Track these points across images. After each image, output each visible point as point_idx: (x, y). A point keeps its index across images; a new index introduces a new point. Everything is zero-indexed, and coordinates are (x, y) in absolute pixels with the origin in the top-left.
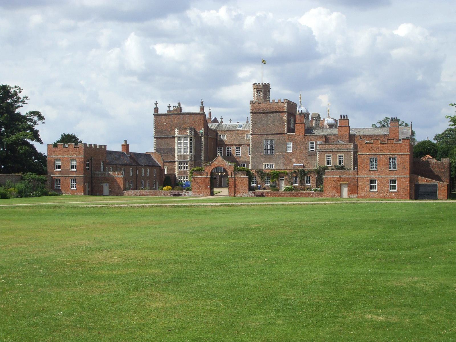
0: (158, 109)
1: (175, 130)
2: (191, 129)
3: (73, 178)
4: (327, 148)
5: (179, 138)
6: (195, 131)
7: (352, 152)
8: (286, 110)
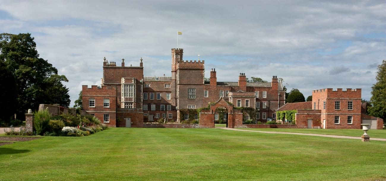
1: (122, 80)
2: (135, 79)
3: (106, 114)
4: (238, 95)
6: (137, 80)
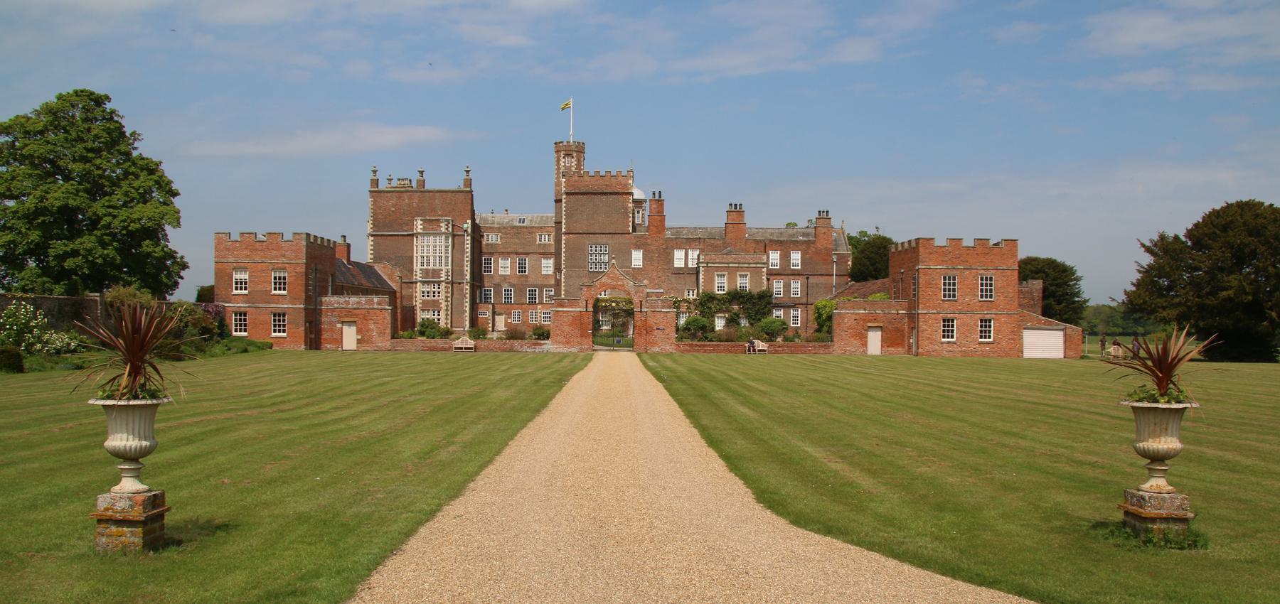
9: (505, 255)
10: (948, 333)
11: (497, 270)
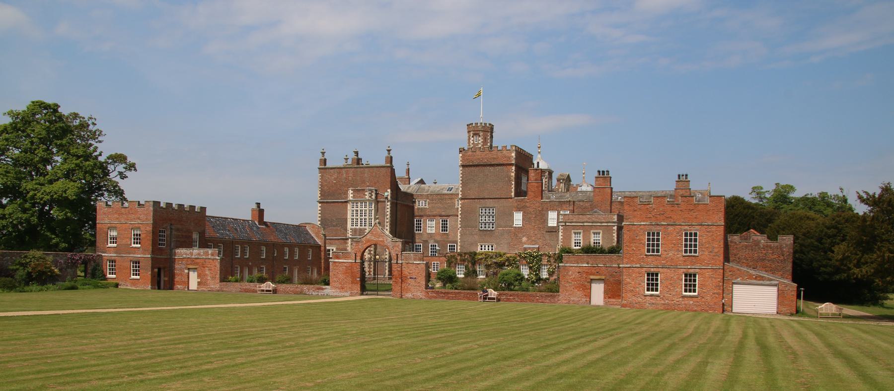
0: (325, 160)
5: (353, 202)
7: (615, 228)
8: (513, 162)
9: (432, 217)
10: (652, 286)
11: (425, 229)
